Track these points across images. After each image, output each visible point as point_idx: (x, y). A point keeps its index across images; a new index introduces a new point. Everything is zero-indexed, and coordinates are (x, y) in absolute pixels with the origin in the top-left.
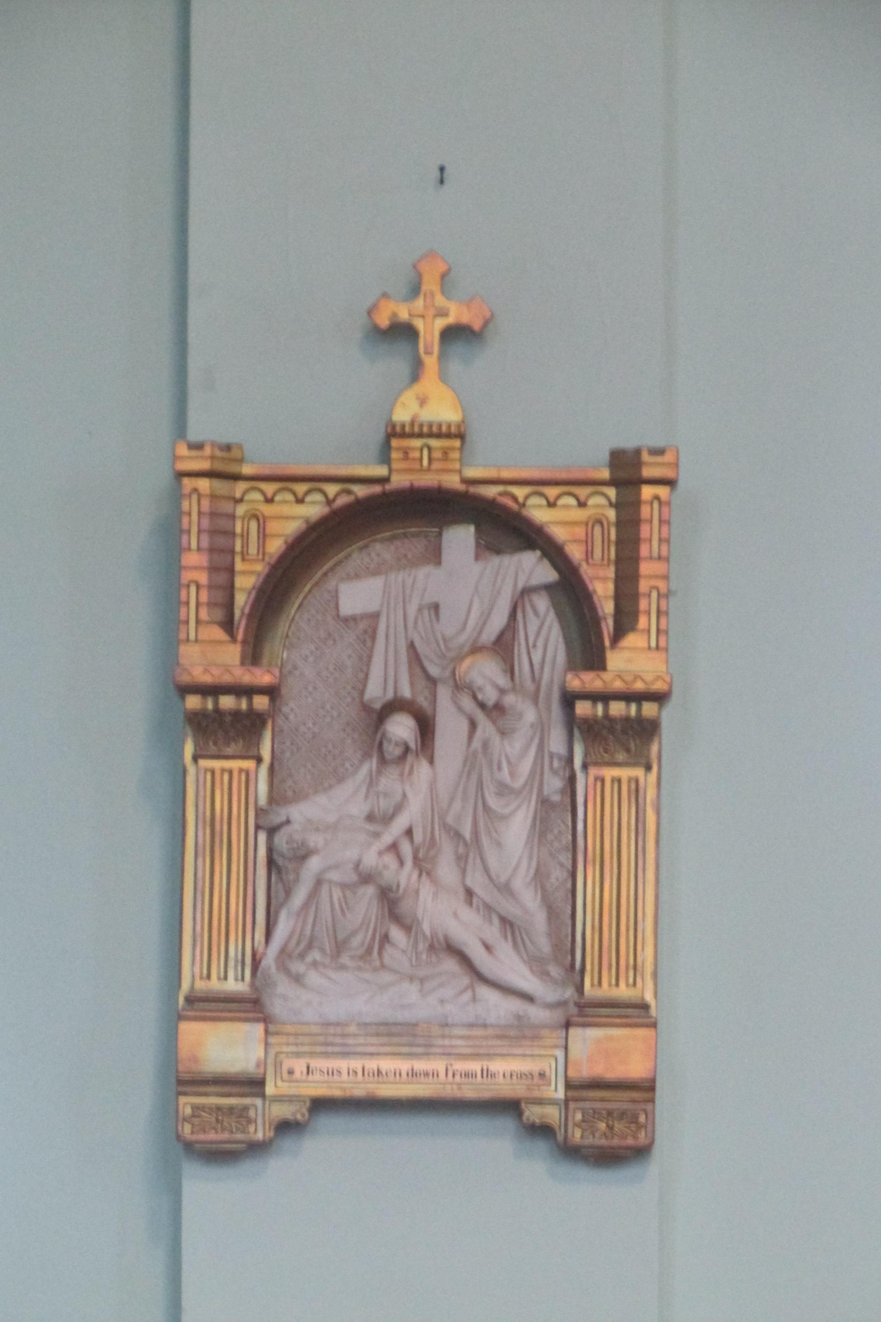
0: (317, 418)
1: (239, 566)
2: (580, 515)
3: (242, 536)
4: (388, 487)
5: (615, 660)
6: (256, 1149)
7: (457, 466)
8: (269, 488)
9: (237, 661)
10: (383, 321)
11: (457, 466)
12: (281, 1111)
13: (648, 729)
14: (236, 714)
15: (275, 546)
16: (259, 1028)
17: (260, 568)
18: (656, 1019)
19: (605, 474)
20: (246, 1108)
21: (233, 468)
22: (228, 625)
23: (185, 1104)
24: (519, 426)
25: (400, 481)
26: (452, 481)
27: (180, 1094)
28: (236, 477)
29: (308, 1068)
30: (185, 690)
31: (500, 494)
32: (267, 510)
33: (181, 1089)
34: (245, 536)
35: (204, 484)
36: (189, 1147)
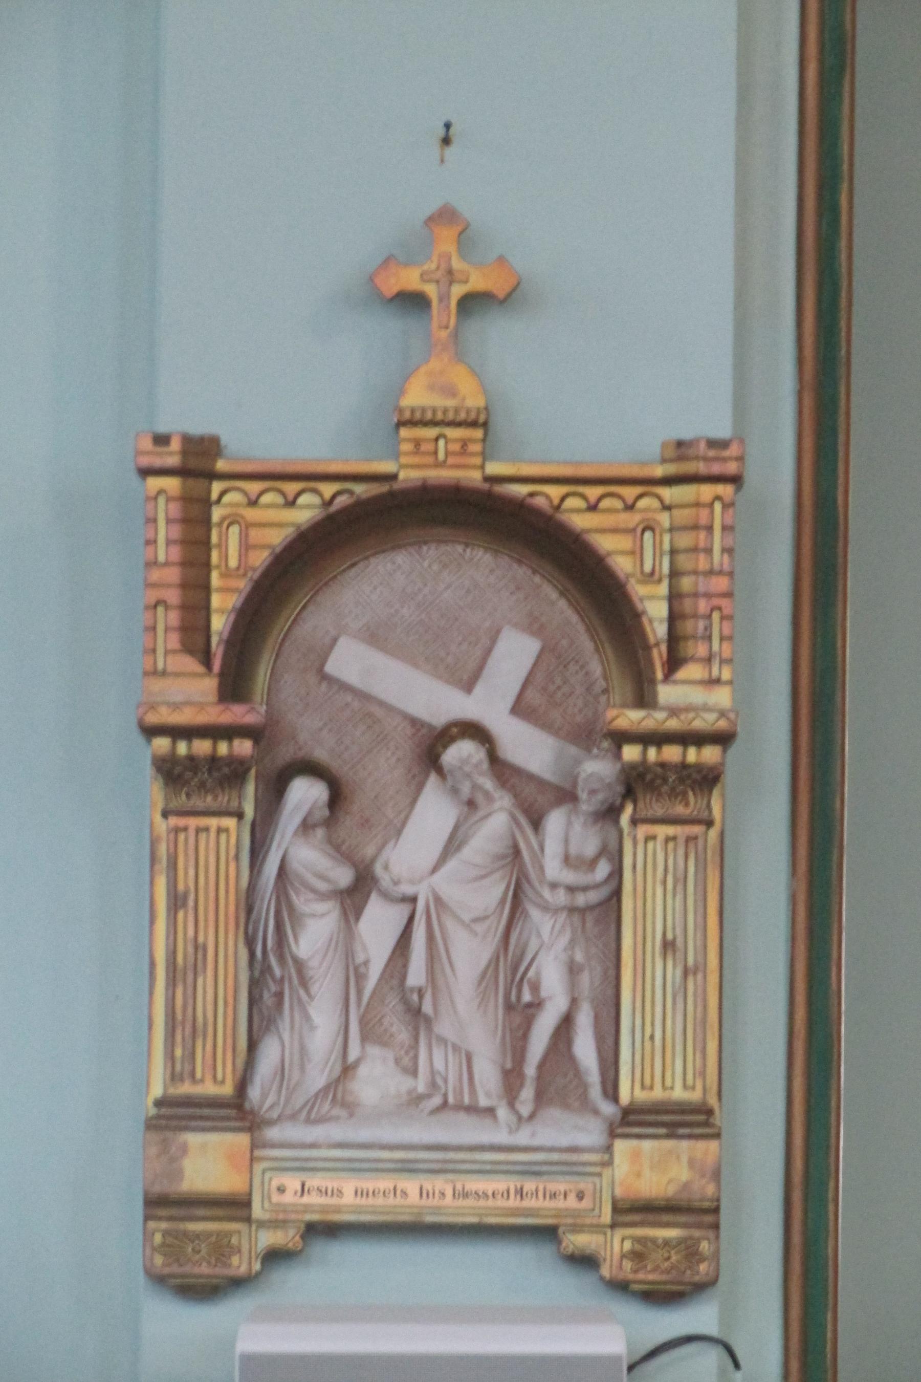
2: (632, 519)
3: (661, 556)
4: (396, 486)
5: (666, 693)
6: (237, 1283)
8: (254, 487)
9: (213, 697)
10: (392, 284)
11: (478, 461)
12: (267, 1239)
13: (707, 779)
14: (213, 760)
15: (260, 559)
16: (243, 1139)
17: (243, 585)
18: (720, 1128)
19: (659, 471)
20: (229, 1234)
22: (207, 661)
25: (409, 476)
26: (473, 477)
28: (214, 476)
29: (303, 1186)
30: (151, 731)
31: (532, 495)
32: (251, 514)
34: (223, 546)
35: (172, 484)
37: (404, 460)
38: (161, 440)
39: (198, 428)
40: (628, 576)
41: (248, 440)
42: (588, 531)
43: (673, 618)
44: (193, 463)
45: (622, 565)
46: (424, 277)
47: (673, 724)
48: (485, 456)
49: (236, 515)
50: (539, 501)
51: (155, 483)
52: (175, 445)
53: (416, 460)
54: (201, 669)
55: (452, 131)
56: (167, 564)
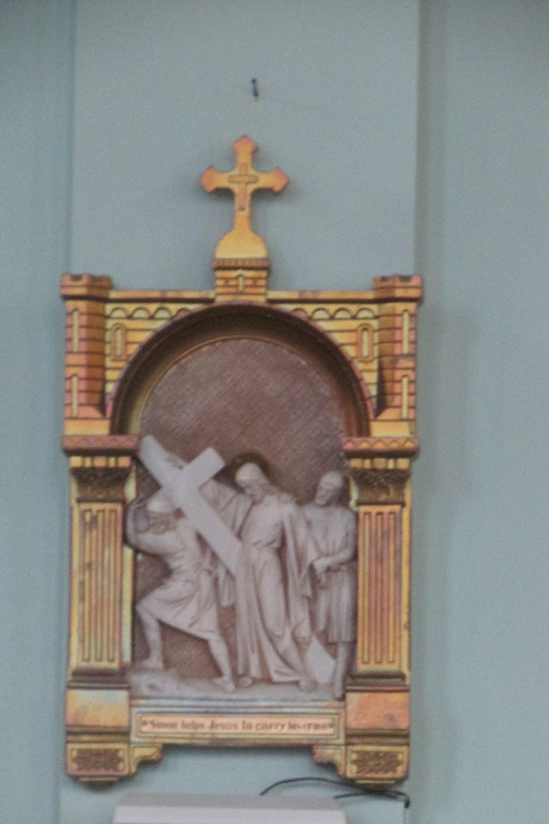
0: (159, 261)
1: (109, 363)
4: (214, 305)
6: (126, 780)
7: (262, 290)
13: (400, 479)
14: (107, 470)
15: (133, 349)
19: (370, 295)
20: (117, 751)
21: (103, 294)
22: (101, 407)
23: (72, 750)
24: (320, 262)
25: (221, 300)
26: (260, 300)
27: (68, 742)
28: (107, 300)
33: (71, 738)
35: (82, 305)
36: (75, 779)
37: (219, 290)
38: (77, 278)
39: (98, 272)
40: (353, 358)
41: (129, 278)
42: (330, 331)
43: (381, 382)
44: (95, 292)
45: (350, 351)
46: (231, 180)
47: (379, 446)
48: (268, 287)
49: (121, 324)
50: (301, 315)
51: (71, 304)
52: (84, 281)
53: (226, 290)
54: (97, 414)
55: (260, 83)
56: (79, 353)
